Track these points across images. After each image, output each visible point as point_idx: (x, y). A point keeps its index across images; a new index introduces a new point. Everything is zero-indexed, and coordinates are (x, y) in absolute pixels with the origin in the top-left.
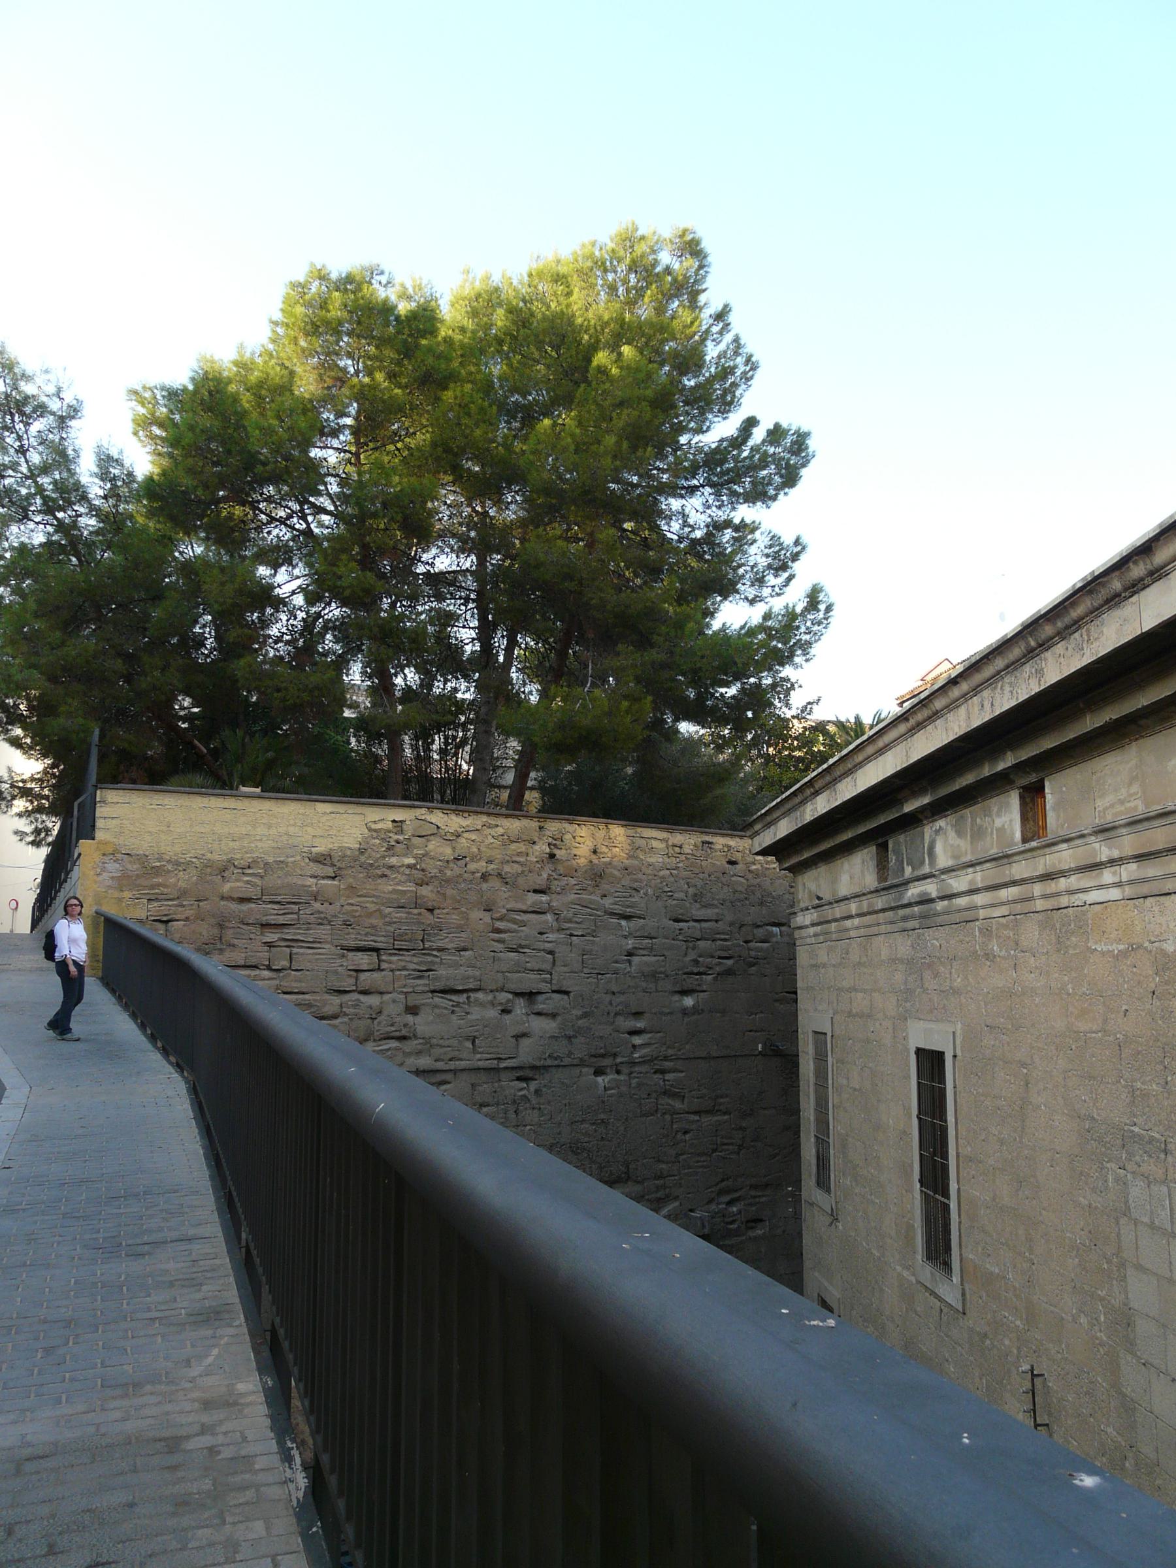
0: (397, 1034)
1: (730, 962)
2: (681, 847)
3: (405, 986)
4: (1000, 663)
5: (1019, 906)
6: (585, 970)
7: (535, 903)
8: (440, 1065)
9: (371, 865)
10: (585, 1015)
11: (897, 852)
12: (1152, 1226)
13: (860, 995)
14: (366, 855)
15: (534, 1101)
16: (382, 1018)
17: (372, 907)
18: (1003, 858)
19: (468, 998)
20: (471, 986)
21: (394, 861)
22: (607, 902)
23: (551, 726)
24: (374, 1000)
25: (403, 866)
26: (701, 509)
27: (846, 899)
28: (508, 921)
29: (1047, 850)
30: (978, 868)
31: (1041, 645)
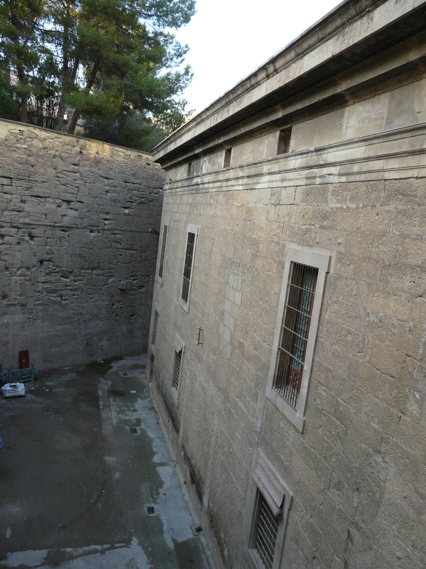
0: (17, 209)
1: (143, 200)
2: (130, 156)
3: (21, 193)
4: (219, 105)
5: (219, 189)
6: (90, 195)
7: (73, 169)
8: (33, 222)
9: (10, 146)
10: (88, 211)
11: (193, 167)
12: (233, 288)
13: (178, 214)
14: (8, 141)
15: (67, 239)
16: (12, 203)
17: (9, 162)
18: (217, 173)
19: (45, 200)
20: (46, 196)
21: (19, 145)
22: (100, 172)
23: (83, 102)
24: (9, 196)
25: (22, 148)
26: (152, 25)
27: (178, 181)
28: (62, 174)
29: (228, 171)
30: (211, 175)
31: (230, 102)
